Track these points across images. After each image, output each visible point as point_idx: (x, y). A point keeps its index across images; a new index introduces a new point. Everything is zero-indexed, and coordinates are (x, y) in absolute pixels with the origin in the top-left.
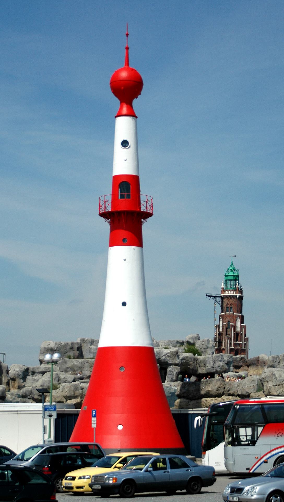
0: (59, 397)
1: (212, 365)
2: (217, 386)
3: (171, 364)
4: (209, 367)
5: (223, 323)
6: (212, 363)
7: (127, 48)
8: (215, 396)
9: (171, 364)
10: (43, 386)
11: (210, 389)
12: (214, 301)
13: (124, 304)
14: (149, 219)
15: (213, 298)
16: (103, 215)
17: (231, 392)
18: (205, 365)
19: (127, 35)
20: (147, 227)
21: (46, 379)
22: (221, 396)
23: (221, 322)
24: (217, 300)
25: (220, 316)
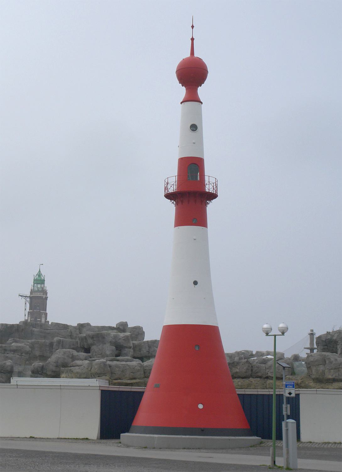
0: (84, 373)
1: (148, 350)
2: (245, 368)
3: (127, 347)
4: (145, 352)
5: (31, 318)
6: (147, 348)
7: (192, 39)
8: (243, 378)
9: (127, 347)
10: (57, 362)
11: (238, 371)
12: (25, 300)
13: (195, 283)
14: (214, 201)
15: (24, 297)
16: (169, 196)
17: (260, 374)
18: (140, 349)
19: (193, 27)
20: (212, 208)
21: (59, 356)
22: (249, 378)
23: (29, 318)
24: (27, 300)
25: (28, 312)
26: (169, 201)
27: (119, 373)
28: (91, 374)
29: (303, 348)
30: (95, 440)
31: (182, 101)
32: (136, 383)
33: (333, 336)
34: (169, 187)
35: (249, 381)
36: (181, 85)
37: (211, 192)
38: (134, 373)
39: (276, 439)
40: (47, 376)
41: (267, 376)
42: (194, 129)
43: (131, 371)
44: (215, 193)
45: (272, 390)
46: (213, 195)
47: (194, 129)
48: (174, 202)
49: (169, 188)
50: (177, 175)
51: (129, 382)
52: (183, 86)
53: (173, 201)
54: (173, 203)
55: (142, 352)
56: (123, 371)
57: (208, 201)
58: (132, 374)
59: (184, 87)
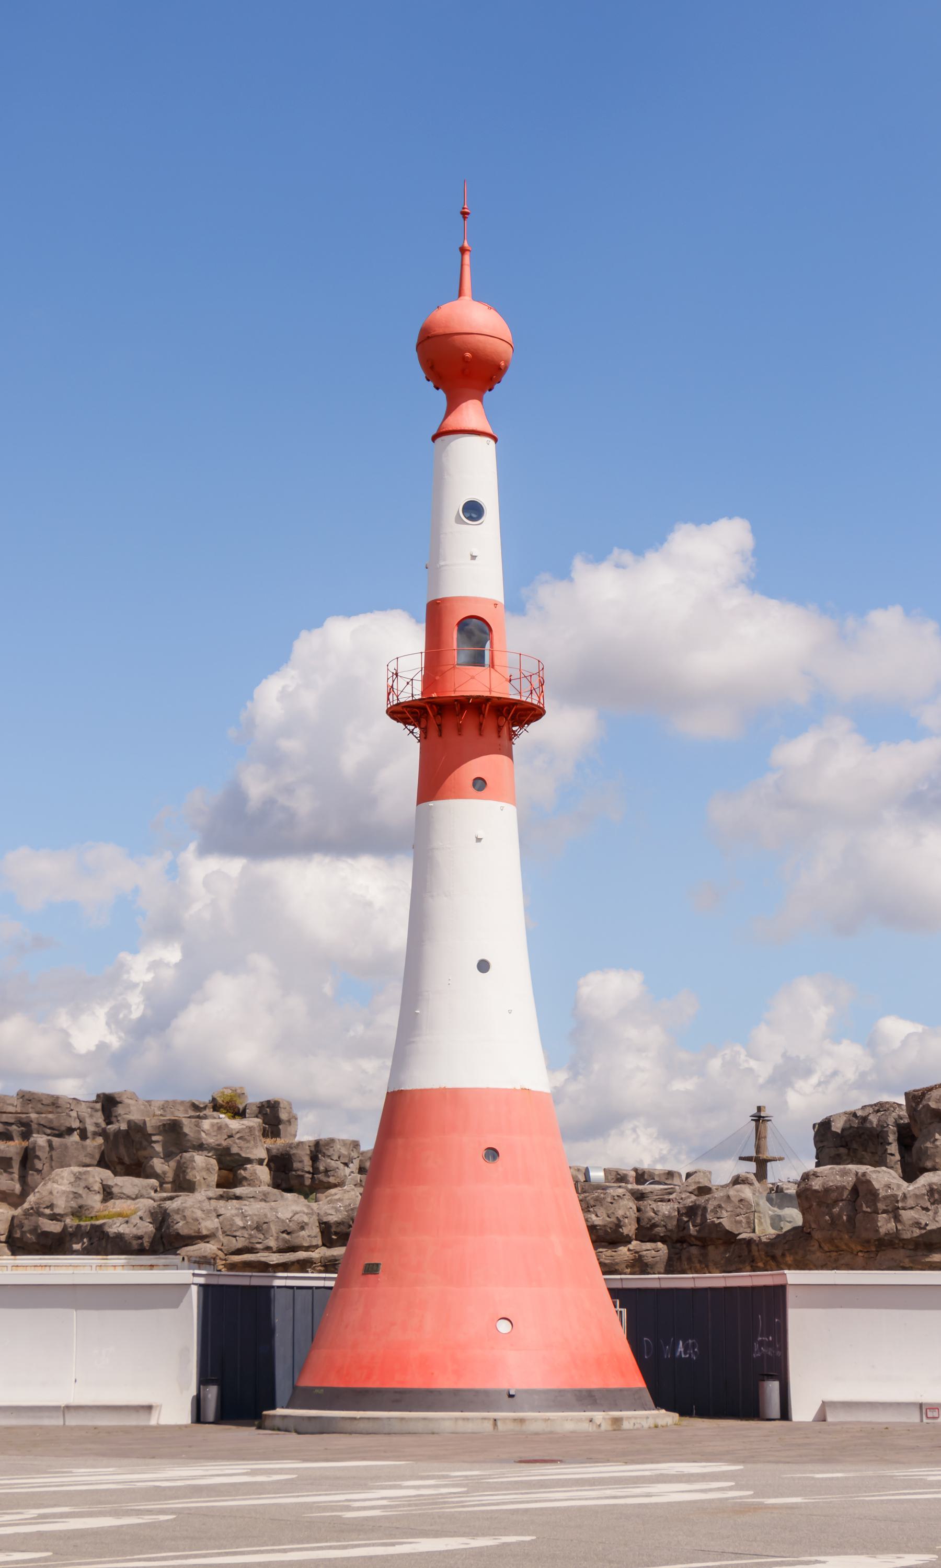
14: (534, 728)
16: (402, 713)
26: (401, 725)
27: (906, 1215)
28: (162, 1238)
29: (499, 1162)
30: (186, 1426)
31: (435, 432)
32: (298, 1261)
33: (864, 1119)
34: (401, 684)
35: (629, 1250)
36: (431, 384)
37: (526, 702)
38: (288, 1233)
39: (751, 1409)
40: (23, 1248)
41: (681, 1234)
42: (474, 516)
43: (283, 1229)
44: (535, 702)
45: (335, 1275)
46: (534, 709)
47: (474, 516)
48: (417, 730)
49: (400, 689)
50: (424, 650)
51: (275, 1258)
52: (438, 389)
53: (411, 727)
54: (412, 732)
55: (665, 1152)
56: (258, 1228)
57: (514, 729)
58: (285, 1235)
59: (440, 390)
